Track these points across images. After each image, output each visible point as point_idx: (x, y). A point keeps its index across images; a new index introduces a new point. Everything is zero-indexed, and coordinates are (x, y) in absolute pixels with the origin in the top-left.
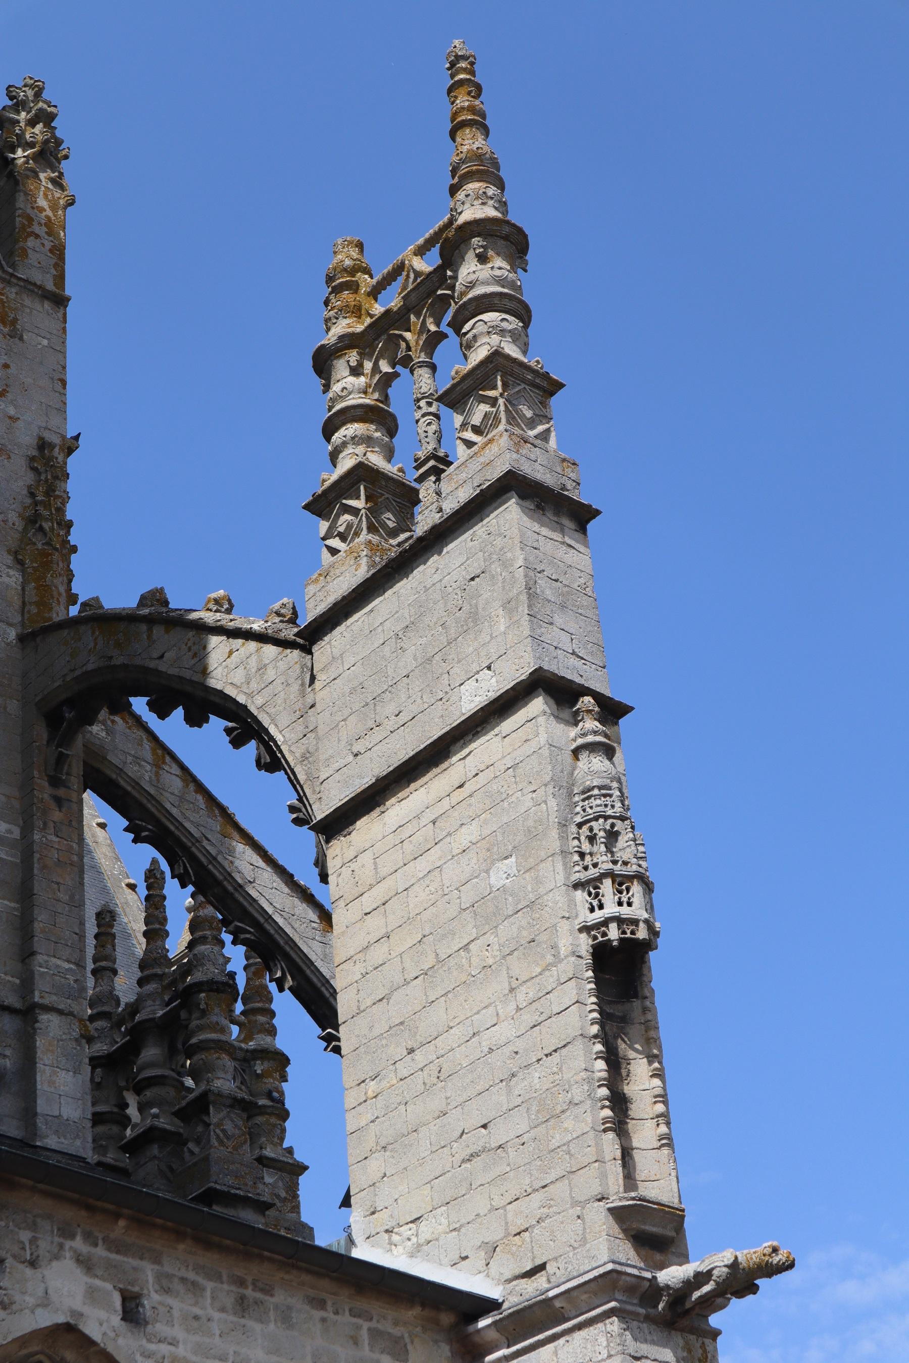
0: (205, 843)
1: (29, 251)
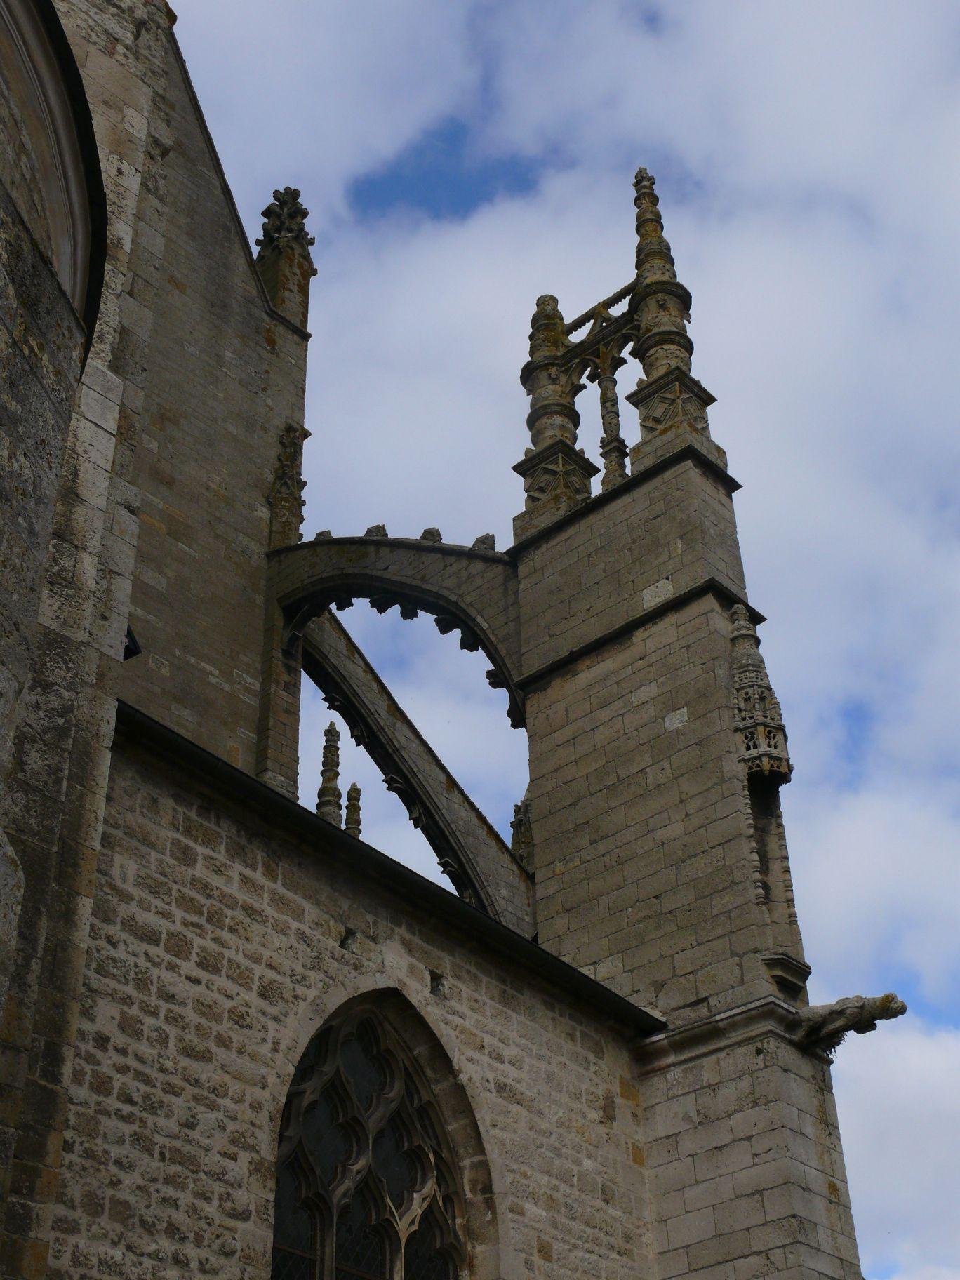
0: (377, 716)
1: (286, 300)
